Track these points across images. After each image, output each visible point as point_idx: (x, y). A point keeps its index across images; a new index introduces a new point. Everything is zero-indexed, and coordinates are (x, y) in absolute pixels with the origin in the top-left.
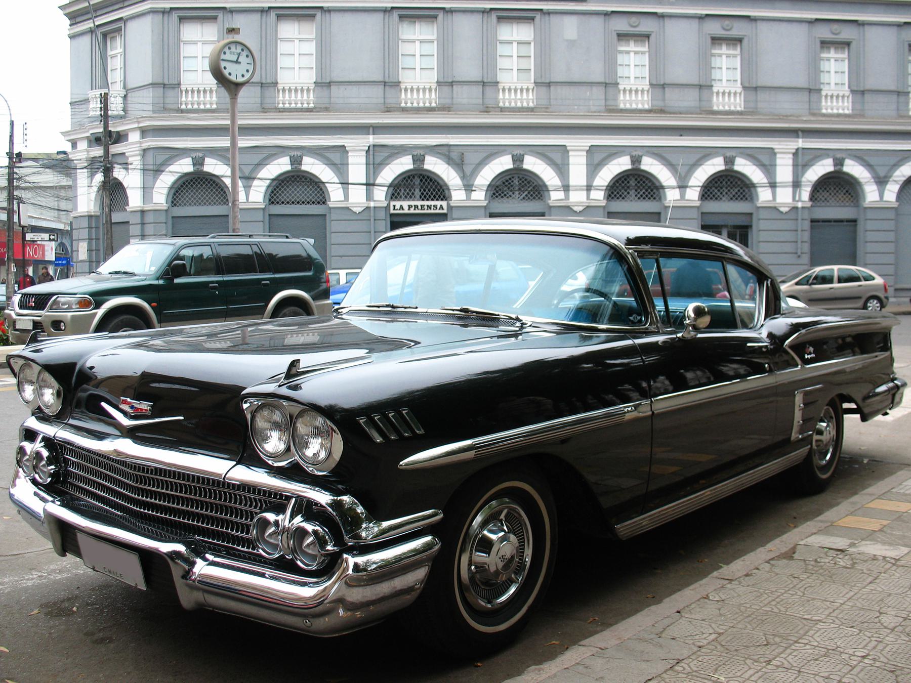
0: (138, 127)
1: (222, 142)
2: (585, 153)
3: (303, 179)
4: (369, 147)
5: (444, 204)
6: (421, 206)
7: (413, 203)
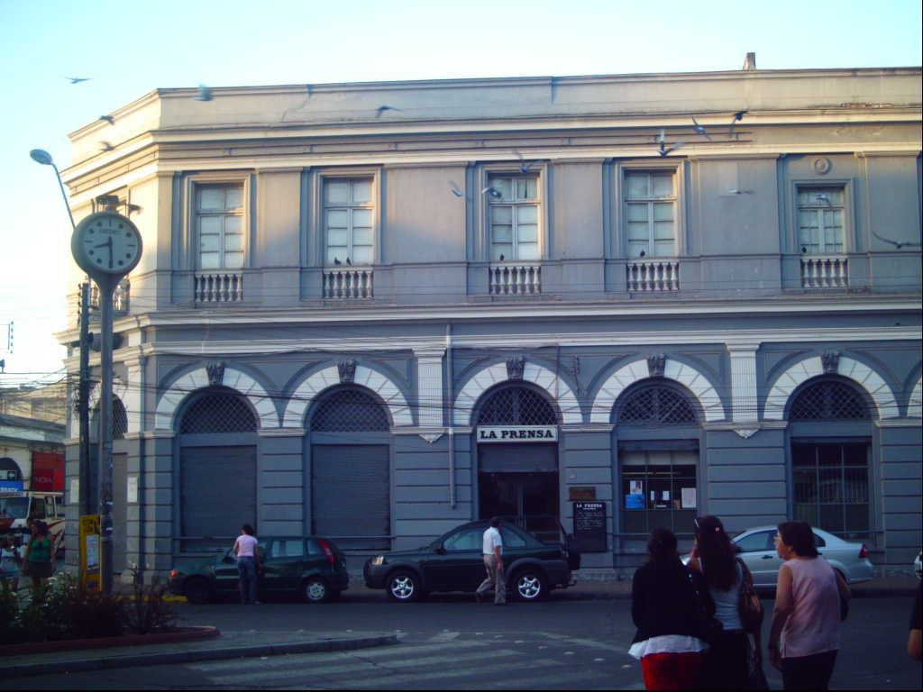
0: (139, 328)
1: (244, 347)
2: (753, 354)
3: (358, 396)
4: (446, 352)
5: (553, 430)
6: (520, 432)
7: (508, 428)
